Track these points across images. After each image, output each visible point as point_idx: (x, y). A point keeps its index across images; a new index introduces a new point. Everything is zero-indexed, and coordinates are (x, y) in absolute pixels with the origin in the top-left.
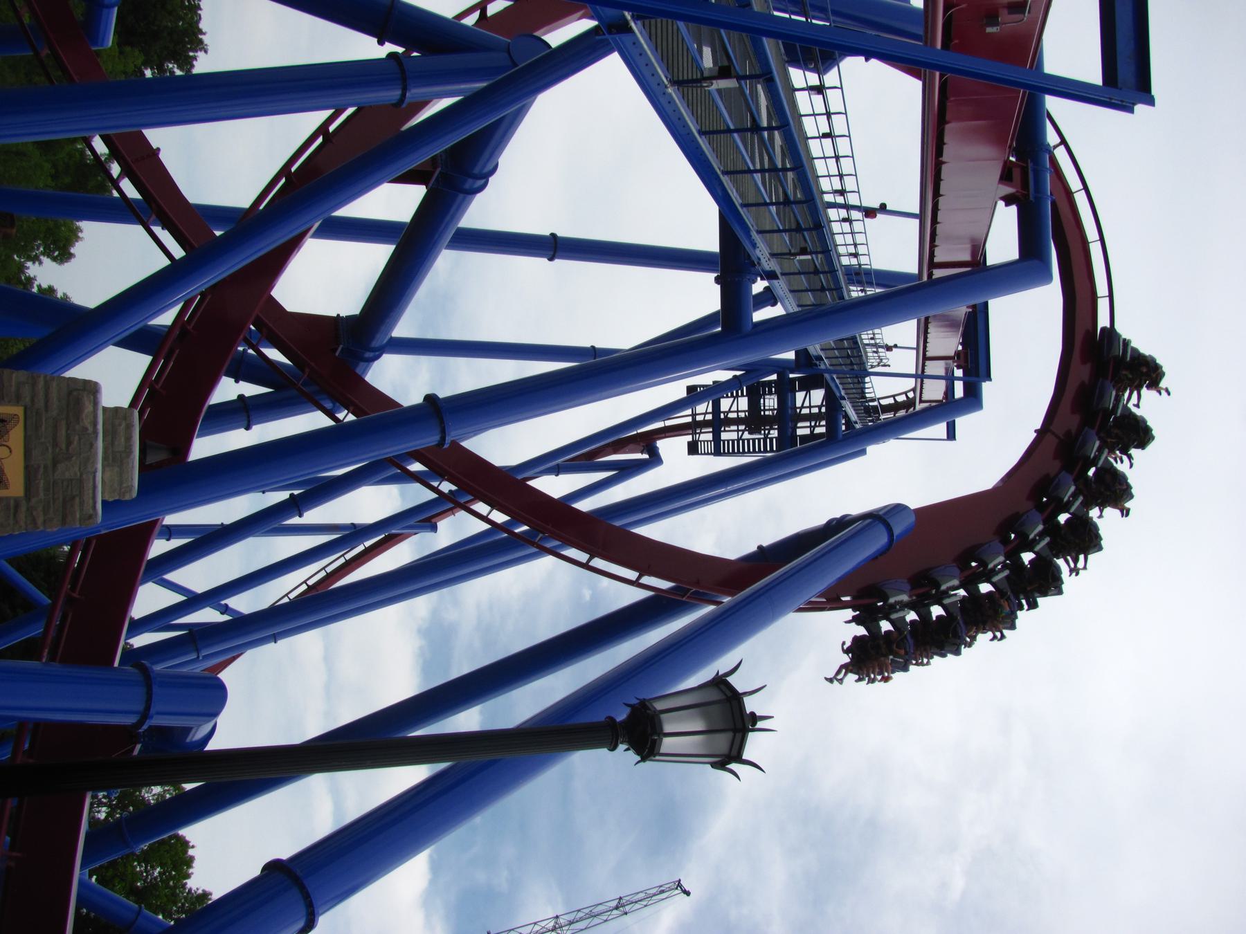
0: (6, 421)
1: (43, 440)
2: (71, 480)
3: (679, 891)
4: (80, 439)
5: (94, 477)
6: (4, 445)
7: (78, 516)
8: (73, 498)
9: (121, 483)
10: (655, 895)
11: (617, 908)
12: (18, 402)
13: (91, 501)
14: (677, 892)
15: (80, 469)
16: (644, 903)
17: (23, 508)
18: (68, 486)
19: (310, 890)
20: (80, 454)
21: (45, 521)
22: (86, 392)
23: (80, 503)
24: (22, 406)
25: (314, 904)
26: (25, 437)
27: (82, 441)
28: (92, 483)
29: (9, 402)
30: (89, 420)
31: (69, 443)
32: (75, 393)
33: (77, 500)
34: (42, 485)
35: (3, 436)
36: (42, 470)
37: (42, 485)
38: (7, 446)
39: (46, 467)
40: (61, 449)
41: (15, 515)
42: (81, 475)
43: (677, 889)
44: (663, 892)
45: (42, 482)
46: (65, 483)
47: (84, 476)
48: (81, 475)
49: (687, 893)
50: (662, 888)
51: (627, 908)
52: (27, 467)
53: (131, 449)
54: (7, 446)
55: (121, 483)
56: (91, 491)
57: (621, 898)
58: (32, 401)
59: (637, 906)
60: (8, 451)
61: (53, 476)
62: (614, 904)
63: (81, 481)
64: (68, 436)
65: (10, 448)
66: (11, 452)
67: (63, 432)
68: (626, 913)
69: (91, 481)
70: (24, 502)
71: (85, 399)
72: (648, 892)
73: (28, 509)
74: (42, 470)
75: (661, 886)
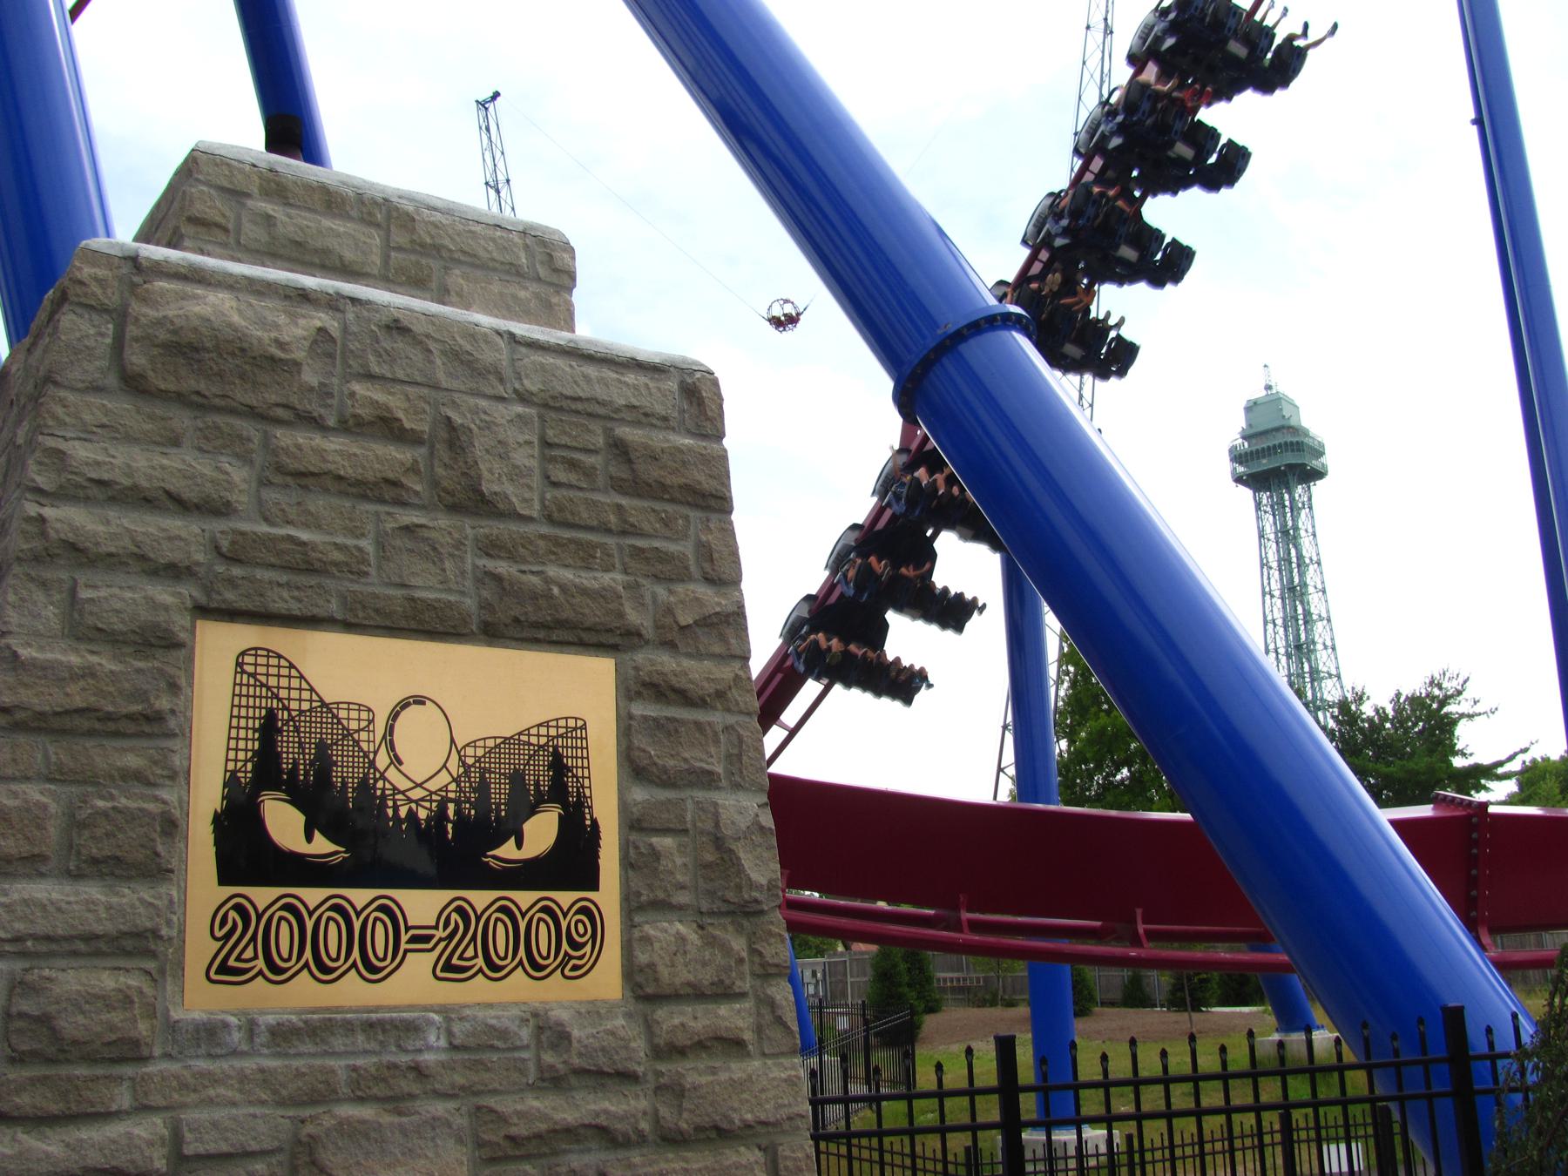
0: (271, 715)
1: (367, 544)
2: (546, 444)
3: (491, 106)
4: (370, 377)
5: (534, 345)
6: (390, 730)
7: (688, 441)
8: (620, 449)
9: (514, 272)
10: (490, 138)
11: (498, 192)
12: (179, 645)
13: (630, 378)
14: (491, 109)
15: (501, 399)
16: (498, 155)
17: (666, 662)
18: (573, 465)
19: (964, 322)
20: (436, 387)
21: (709, 580)
22: (136, 308)
23: (637, 423)
24: (192, 631)
25: (973, 319)
26: (349, 626)
27: (375, 369)
28: (560, 362)
29: (174, 688)
30: (282, 319)
31: (387, 427)
32: (137, 359)
33: (626, 432)
34: (568, 575)
35: (348, 733)
36: (502, 567)
37: (568, 575)
38: (394, 716)
39: (490, 548)
40: (413, 469)
41: (700, 703)
42: (523, 398)
43: (486, 109)
44: (488, 129)
45: (553, 571)
46: (560, 474)
47: (532, 385)
48: (523, 398)
49: (496, 95)
50: (484, 128)
51: (501, 178)
52: (492, 634)
53: (374, 202)
54: (394, 716)
55: (514, 272)
56: (591, 371)
57: (487, 183)
58: (174, 572)
59: (501, 165)
60: (414, 709)
61: (530, 519)
62: (492, 192)
63: (552, 405)
64: (351, 426)
65: (404, 705)
66: (420, 701)
67: (335, 449)
68: (508, 181)
69: (549, 360)
70: (640, 657)
71: (171, 312)
72: (485, 146)
73: (670, 645)
74: (502, 567)
75: (480, 128)
